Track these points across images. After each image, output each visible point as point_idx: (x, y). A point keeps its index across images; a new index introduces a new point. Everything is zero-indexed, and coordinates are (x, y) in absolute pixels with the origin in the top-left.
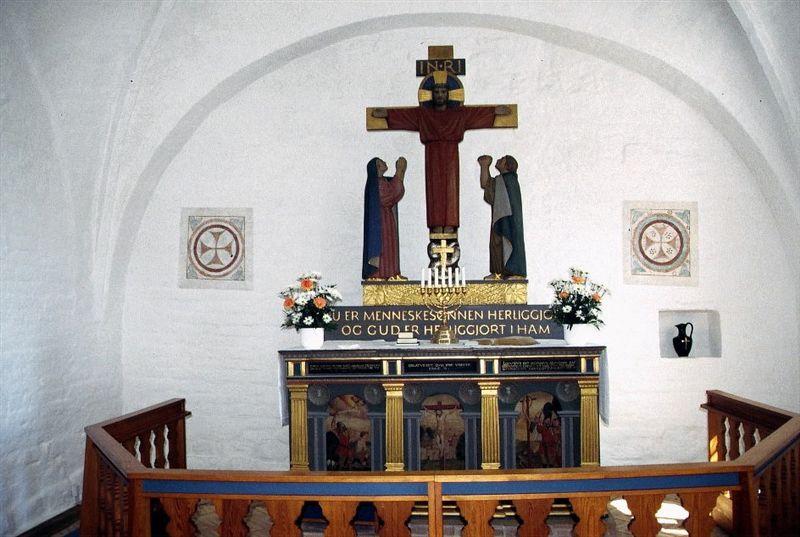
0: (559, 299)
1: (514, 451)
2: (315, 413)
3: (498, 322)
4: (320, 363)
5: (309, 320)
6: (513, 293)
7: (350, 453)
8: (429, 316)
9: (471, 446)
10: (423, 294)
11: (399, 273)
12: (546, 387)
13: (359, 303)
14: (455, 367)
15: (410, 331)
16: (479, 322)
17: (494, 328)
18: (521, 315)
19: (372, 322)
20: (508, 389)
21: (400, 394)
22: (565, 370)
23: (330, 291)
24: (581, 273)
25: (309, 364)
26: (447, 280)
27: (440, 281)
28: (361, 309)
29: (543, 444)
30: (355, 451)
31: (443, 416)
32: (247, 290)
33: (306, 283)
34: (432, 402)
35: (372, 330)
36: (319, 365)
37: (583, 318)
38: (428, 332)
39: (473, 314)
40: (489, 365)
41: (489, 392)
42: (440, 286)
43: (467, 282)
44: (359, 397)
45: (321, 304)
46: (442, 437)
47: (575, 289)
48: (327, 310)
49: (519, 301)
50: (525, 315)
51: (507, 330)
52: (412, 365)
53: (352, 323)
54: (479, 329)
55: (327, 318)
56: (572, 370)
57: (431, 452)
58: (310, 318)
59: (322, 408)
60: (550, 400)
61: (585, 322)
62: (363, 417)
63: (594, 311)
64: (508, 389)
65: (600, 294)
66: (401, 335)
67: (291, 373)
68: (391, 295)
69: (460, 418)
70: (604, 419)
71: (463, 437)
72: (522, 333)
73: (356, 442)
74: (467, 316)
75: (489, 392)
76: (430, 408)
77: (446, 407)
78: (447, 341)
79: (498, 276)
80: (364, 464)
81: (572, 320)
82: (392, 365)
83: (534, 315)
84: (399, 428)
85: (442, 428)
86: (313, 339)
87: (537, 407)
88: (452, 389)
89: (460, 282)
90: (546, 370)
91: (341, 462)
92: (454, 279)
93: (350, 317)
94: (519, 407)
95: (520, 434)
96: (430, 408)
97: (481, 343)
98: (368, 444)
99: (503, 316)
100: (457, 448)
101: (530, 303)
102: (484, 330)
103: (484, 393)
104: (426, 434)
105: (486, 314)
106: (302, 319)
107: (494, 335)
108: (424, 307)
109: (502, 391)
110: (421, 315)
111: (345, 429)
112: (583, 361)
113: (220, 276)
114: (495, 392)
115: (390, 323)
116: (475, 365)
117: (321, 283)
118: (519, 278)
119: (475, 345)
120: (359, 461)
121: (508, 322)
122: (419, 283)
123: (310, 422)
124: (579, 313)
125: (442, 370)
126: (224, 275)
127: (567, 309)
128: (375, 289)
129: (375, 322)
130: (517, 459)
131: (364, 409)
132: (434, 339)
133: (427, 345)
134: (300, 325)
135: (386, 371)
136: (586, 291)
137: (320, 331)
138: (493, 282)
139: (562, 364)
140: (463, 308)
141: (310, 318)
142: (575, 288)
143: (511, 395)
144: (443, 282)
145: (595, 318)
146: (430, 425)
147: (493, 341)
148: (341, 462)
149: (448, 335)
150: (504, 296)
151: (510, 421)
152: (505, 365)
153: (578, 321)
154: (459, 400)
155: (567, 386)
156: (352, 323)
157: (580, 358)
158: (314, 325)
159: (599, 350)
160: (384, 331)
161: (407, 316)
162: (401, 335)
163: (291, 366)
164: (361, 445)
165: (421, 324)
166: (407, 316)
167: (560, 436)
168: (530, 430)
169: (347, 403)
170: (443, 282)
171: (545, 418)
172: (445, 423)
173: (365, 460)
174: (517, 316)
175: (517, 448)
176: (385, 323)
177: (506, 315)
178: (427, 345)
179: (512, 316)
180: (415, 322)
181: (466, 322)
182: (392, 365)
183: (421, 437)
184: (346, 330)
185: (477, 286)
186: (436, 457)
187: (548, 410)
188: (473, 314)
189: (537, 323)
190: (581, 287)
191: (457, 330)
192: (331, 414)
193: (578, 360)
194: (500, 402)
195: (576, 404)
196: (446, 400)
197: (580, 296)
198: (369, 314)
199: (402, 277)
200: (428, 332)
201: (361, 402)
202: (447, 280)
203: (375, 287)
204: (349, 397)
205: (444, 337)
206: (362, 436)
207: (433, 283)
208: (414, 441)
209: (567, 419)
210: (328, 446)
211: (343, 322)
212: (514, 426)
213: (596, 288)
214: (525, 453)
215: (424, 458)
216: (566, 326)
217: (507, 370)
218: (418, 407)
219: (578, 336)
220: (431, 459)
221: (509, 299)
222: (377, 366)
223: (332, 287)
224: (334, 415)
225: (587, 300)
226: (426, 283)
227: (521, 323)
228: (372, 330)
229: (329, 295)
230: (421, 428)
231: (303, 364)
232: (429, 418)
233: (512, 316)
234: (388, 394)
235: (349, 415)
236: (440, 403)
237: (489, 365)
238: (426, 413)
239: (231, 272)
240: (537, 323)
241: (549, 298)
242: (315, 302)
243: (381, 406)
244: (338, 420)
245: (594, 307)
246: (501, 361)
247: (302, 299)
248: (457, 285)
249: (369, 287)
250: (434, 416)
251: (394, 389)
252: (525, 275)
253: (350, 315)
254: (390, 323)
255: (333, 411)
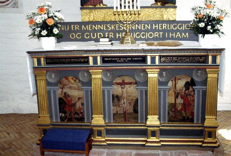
0: (197, 18)
1: (167, 108)
2: (51, 87)
3: (159, 31)
4: (52, 58)
5: (44, 33)
6: (168, 14)
7: (73, 109)
8: (119, 28)
9: (142, 107)
10: (115, 15)
11: (102, 2)
12: (187, 72)
13: (80, 20)
14: (132, 60)
15: (108, 37)
16: (147, 31)
17: (156, 34)
18: (172, 26)
19: (87, 31)
20: (164, 73)
21: (100, 76)
22: (199, 62)
23: (57, 14)
24: (211, 2)
25: (47, 59)
26: (129, 6)
27: (125, 6)
28: (80, 24)
29: (184, 105)
30: (75, 108)
31: (125, 89)
32: (20, 13)
33: (41, 9)
34: (119, 80)
35: (87, 36)
36: (53, 60)
37: (211, 31)
38: (119, 37)
39: (144, 26)
40: (153, 59)
41: (153, 75)
42: (125, 10)
43: (141, 7)
44: (76, 78)
45: (51, 22)
46: (125, 100)
47: (208, 13)
48: (56, 25)
49: (171, 19)
50: (175, 26)
51: (164, 35)
52: (107, 59)
53: (76, 32)
54: (148, 35)
55: (56, 31)
56: (204, 62)
57: (118, 109)
58: (45, 31)
59: (55, 84)
60: (189, 80)
61: (212, 33)
62: (79, 89)
63: (218, 27)
64: (164, 73)
65: (223, 16)
66: (101, 40)
67: (36, 65)
68: (97, 15)
69: (136, 90)
70: (220, 91)
71: (137, 100)
72: (172, 38)
73: (76, 103)
74: (141, 27)
75: (153, 75)
76: (118, 84)
77: (127, 84)
78: (129, 43)
79: (159, 4)
80: (81, 115)
81: (204, 31)
82: (95, 59)
83: (180, 27)
84: (99, 94)
85: (125, 95)
86: (49, 44)
87: (181, 84)
88: (131, 73)
89: (137, 8)
90: (187, 62)
91: (68, 115)
92: (133, 6)
93: (74, 28)
94: (170, 84)
95: (171, 99)
96: (118, 84)
97: (149, 45)
98: (83, 104)
99: (162, 27)
100: (134, 107)
101: (178, 19)
102: (151, 35)
103: (149, 75)
104: (116, 99)
105: (152, 26)
106: (40, 31)
107: (155, 39)
108: (115, 22)
109: (160, 74)
110: (115, 27)
111: (69, 96)
112: (210, 58)
113: (5, 6)
114: (156, 75)
115: (97, 31)
116: (143, 59)
117: (52, 10)
118: (171, 5)
119: (145, 47)
120: (78, 114)
121: (164, 31)
122: (112, 8)
123: (49, 93)
124: (209, 27)
125: (125, 62)
126: (7, 5)
127: (202, 25)
128: (88, 12)
129: (88, 31)
130: (169, 113)
131: (80, 84)
132: (122, 41)
133: (117, 46)
134: (40, 36)
135: (149, 62)
136: (214, 14)
137: (52, 39)
138: (156, 8)
139: (197, 59)
140: (139, 23)
141: (45, 31)
142: (208, 11)
143: (168, 74)
144: (127, 7)
145: (219, 30)
146: (118, 94)
147: (156, 43)
148: (68, 115)
149: (130, 39)
150: (162, 15)
151: (165, 91)
152: (163, 59)
153: (208, 32)
154: (135, 79)
155: (199, 72)
156: (76, 32)
157: (209, 55)
158: (48, 36)
159: (220, 51)
160: (94, 36)
161: (107, 28)
162: (101, 40)
163: (36, 60)
164: (78, 105)
165: (115, 32)
166: (107, 28)
167: (194, 100)
168: (176, 97)
169: (69, 81)
170: (127, 7)
171: (186, 90)
172: (127, 92)
173: (81, 113)
174: (170, 27)
175: (169, 107)
176: (94, 31)
177: (164, 27)
178: (117, 46)
179: (167, 27)
180: (111, 31)
181: (140, 31)
182: (95, 59)
183: (113, 100)
184: (73, 36)
185: (147, 10)
186: (122, 112)
187: (188, 85)
188: (144, 26)
189: (181, 32)
190: (212, 11)
191: (135, 35)
192: (61, 88)
193: (207, 56)
194: (159, 80)
195: (205, 82)
196: (127, 80)
197: (209, 17)
198: (85, 26)
199: (104, 5)
200: (119, 37)
201: (77, 81)
202: (129, 6)
203: (88, 11)
204: (70, 78)
205: (127, 40)
206: (78, 99)
207: (121, 8)
208: (109, 103)
209: (199, 91)
210: (60, 105)
211: (70, 31)
212: (167, 94)
213: (220, 12)
214: (173, 110)
215: (115, 112)
216: (200, 35)
217: (164, 62)
218: (110, 84)
219: (207, 42)
220: (119, 113)
221: (165, 18)
222: (86, 60)
223: (59, 11)
224: (62, 88)
225: (214, 19)
226: (117, 8)
227: (172, 31)
228: (87, 36)
229: (56, 16)
230: (113, 96)
231: (42, 59)
232: (117, 90)
233: (167, 27)
234: (93, 76)
235: (70, 88)
236: (123, 81)
237: (153, 59)
238: (115, 87)
239: (10, 3)
240: (181, 32)
241: (191, 17)
242: (47, 21)
243: (89, 83)
244: (65, 91)
245: (218, 23)
246: (160, 57)
247: (39, 20)
248: (135, 9)
249: (85, 11)
250: (120, 89)
251: (96, 73)
252: (175, 3)
253: (74, 27)
254: (97, 31)
255: (61, 86)
